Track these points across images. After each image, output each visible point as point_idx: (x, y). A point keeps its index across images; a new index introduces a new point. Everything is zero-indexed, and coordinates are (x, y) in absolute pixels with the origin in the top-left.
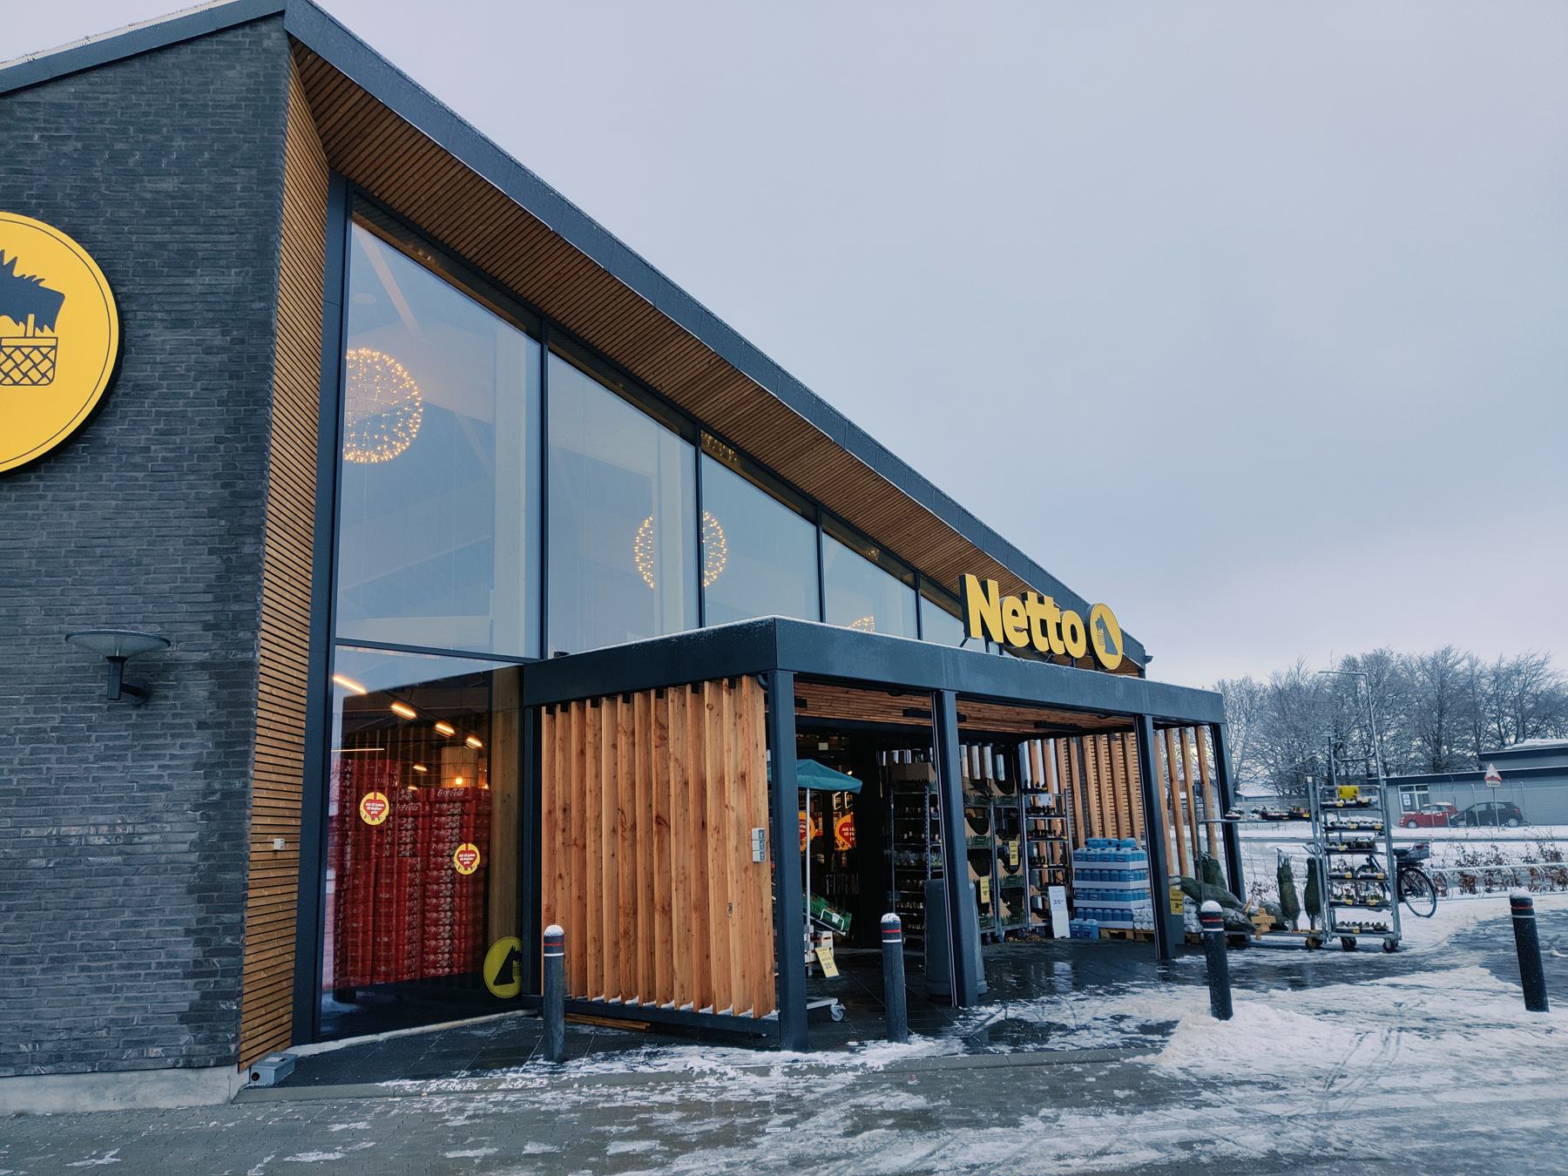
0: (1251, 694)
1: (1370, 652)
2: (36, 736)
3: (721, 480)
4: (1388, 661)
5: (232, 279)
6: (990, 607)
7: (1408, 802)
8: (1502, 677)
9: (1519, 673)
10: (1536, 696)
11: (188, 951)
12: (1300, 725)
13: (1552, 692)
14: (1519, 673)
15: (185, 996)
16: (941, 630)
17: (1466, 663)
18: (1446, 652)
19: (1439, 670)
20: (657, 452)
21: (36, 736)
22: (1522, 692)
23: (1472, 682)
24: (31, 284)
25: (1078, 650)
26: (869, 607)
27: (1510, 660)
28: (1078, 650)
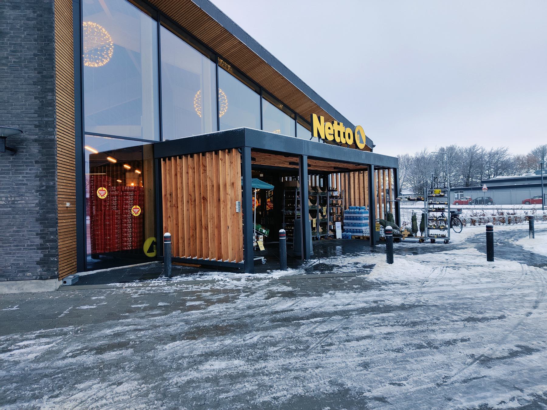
0: (408, 160)
1: (449, 146)
6: (321, 126)
7: (456, 197)
8: (492, 155)
11: (38, 241)
12: (424, 170)
13: (507, 161)
15: (38, 256)
16: (303, 134)
17: (480, 150)
18: (474, 146)
19: (471, 152)
20: (202, 65)
23: (482, 157)
25: (350, 142)
26: (279, 125)
27: (495, 149)
28: (350, 142)
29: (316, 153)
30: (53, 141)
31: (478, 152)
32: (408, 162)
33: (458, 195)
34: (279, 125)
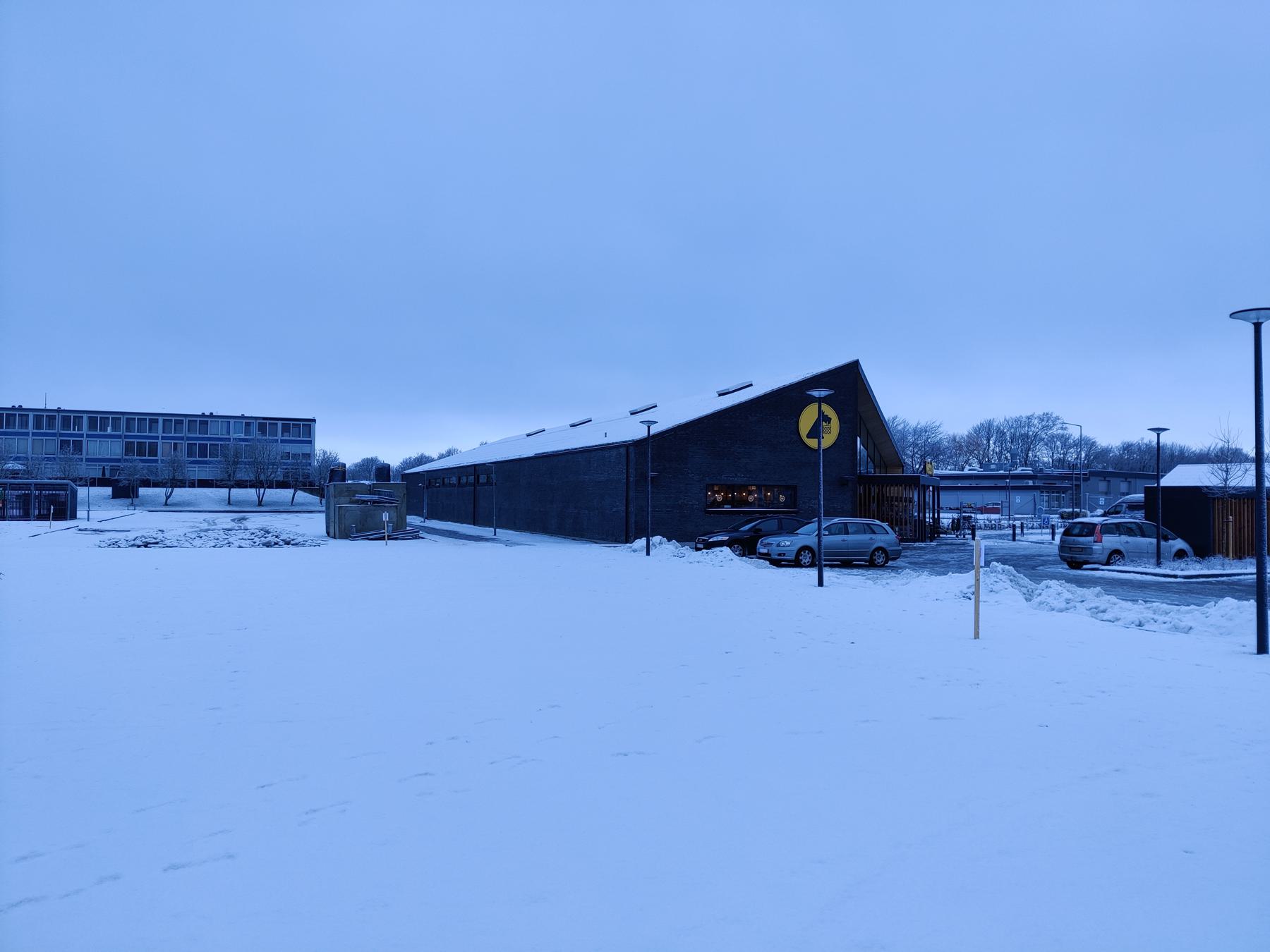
8: (917, 432)
27: (923, 423)
30: (1227, 555)
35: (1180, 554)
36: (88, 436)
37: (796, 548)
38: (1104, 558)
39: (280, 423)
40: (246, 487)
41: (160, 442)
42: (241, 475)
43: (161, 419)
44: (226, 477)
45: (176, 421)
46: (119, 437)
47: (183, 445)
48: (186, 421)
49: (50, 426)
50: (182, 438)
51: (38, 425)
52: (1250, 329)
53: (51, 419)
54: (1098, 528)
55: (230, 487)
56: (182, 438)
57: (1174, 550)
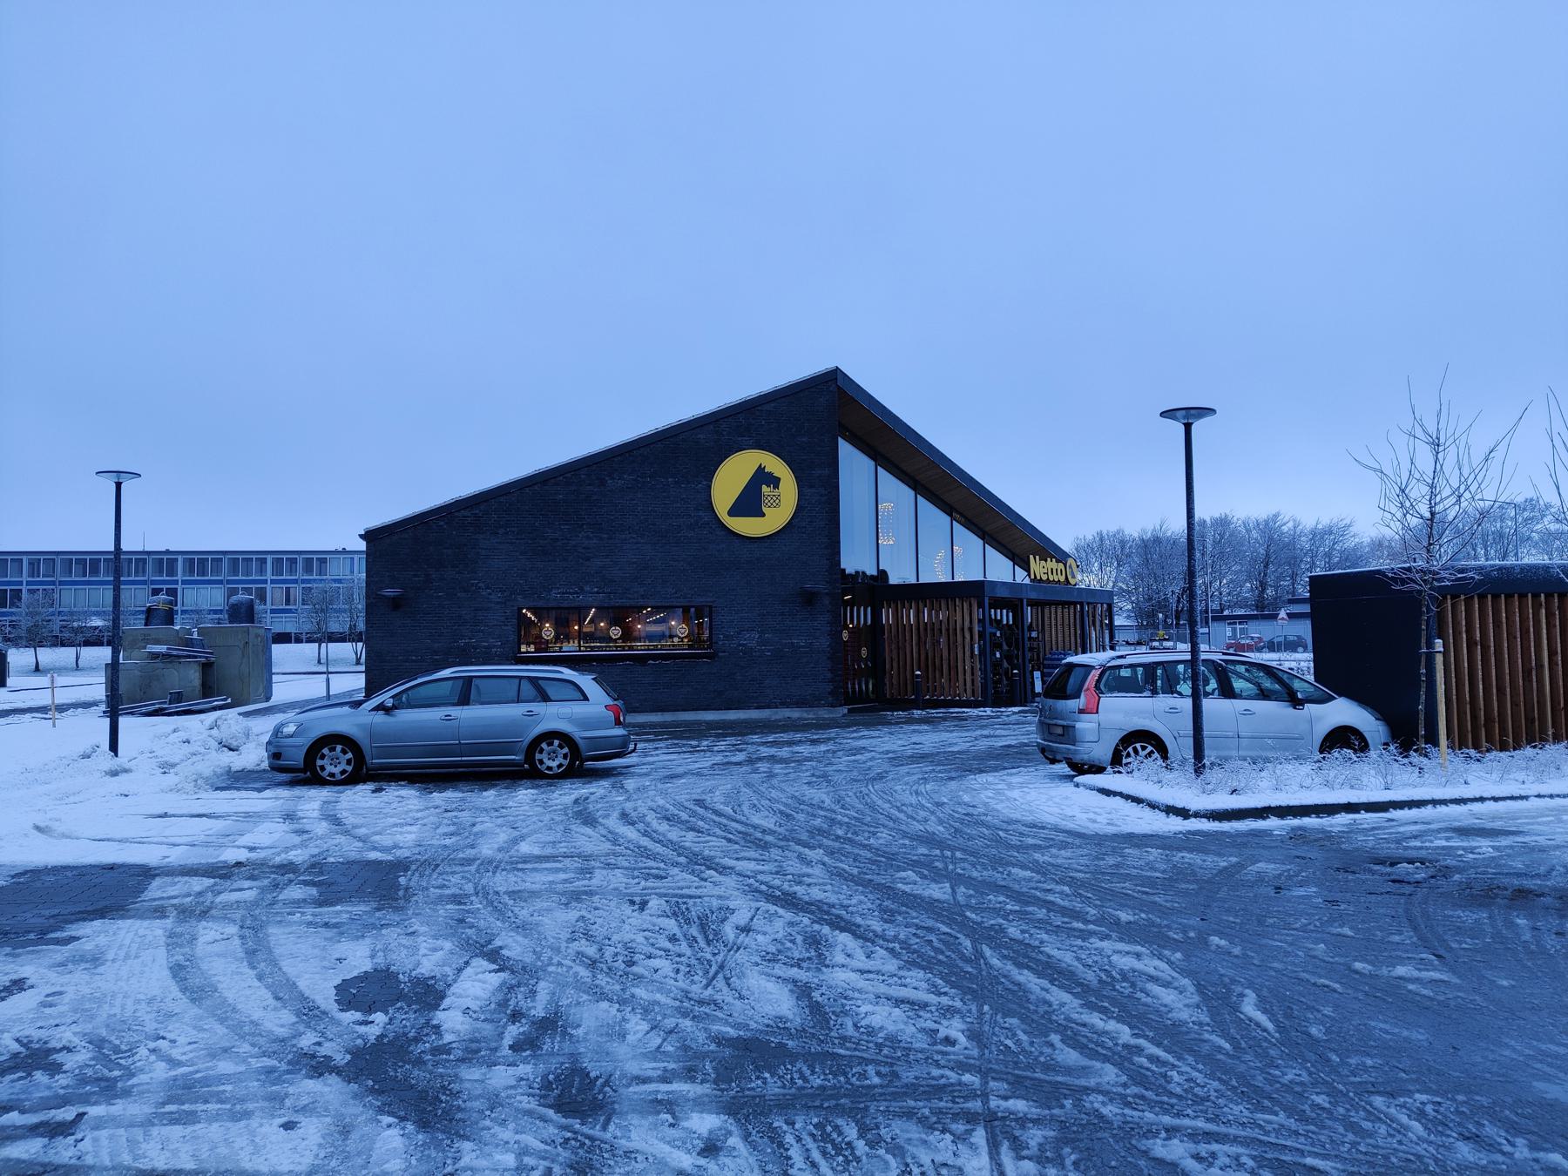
0: (1123, 543)
1: (1217, 515)
2: (782, 614)
3: (963, 534)
4: (1230, 523)
5: (827, 472)
6: (1039, 567)
7: (1229, 633)
8: (1318, 535)
9: (1331, 533)
10: (1342, 552)
11: (829, 675)
12: (1159, 572)
13: (1355, 549)
14: (1331, 533)
15: (830, 688)
16: (1021, 576)
17: (1290, 525)
18: (1276, 516)
19: (1268, 528)
20: (896, 494)
21: (782, 614)
22: (1332, 549)
23: (1294, 538)
24: (770, 474)
25: (1062, 579)
26: (1000, 570)
27: (1325, 521)
28: (1062, 579)
29: (1033, 596)
30: (1544, 740)
31: (1285, 529)
32: (1123, 548)
33: (1234, 630)
34: (1000, 570)
35: (1342, 739)
36: (184, 582)
37: (305, 741)
38: (1101, 751)
39: (25, 558)
40: (289, 642)
41: (269, 586)
42: (334, 627)
43: (269, 558)
44: (315, 629)
45: (286, 561)
46: (220, 582)
47: (297, 591)
48: (300, 558)
49: (216, 571)
50: (295, 581)
51: (278, 569)
52: (1180, 429)
53: (203, 562)
54: (1095, 674)
55: (320, 641)
56: (295, 581)
57: (1323, 729)
